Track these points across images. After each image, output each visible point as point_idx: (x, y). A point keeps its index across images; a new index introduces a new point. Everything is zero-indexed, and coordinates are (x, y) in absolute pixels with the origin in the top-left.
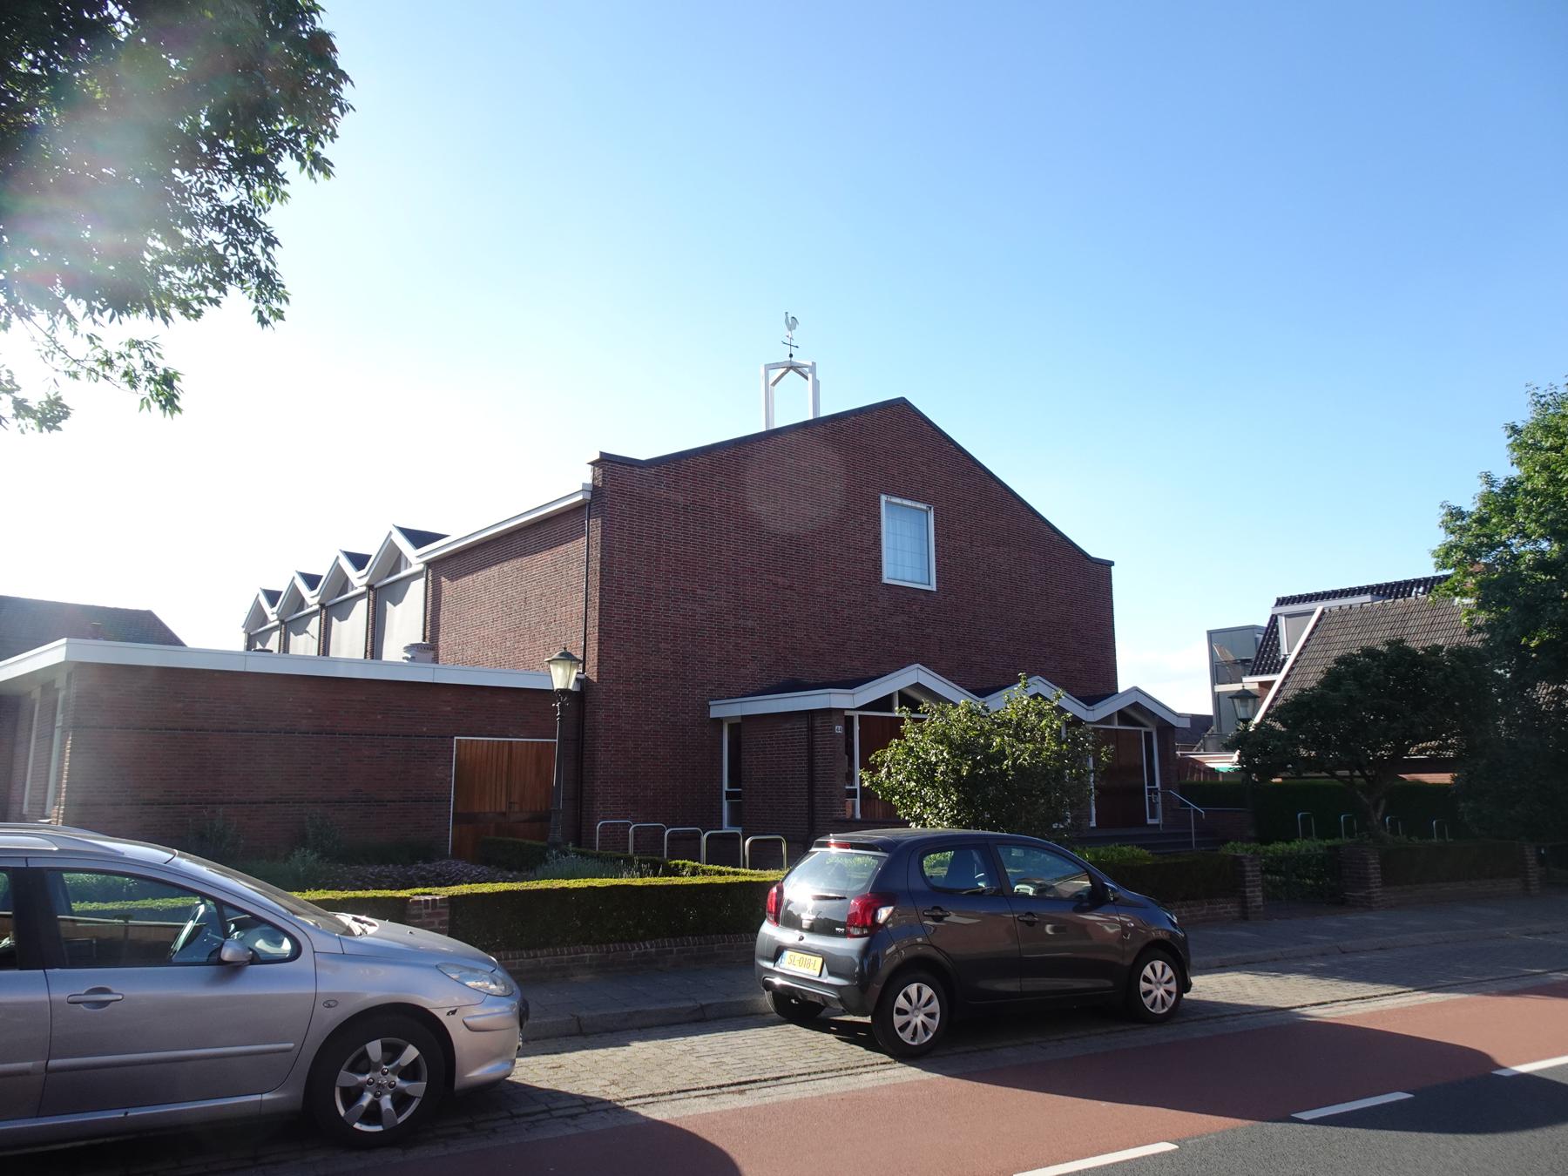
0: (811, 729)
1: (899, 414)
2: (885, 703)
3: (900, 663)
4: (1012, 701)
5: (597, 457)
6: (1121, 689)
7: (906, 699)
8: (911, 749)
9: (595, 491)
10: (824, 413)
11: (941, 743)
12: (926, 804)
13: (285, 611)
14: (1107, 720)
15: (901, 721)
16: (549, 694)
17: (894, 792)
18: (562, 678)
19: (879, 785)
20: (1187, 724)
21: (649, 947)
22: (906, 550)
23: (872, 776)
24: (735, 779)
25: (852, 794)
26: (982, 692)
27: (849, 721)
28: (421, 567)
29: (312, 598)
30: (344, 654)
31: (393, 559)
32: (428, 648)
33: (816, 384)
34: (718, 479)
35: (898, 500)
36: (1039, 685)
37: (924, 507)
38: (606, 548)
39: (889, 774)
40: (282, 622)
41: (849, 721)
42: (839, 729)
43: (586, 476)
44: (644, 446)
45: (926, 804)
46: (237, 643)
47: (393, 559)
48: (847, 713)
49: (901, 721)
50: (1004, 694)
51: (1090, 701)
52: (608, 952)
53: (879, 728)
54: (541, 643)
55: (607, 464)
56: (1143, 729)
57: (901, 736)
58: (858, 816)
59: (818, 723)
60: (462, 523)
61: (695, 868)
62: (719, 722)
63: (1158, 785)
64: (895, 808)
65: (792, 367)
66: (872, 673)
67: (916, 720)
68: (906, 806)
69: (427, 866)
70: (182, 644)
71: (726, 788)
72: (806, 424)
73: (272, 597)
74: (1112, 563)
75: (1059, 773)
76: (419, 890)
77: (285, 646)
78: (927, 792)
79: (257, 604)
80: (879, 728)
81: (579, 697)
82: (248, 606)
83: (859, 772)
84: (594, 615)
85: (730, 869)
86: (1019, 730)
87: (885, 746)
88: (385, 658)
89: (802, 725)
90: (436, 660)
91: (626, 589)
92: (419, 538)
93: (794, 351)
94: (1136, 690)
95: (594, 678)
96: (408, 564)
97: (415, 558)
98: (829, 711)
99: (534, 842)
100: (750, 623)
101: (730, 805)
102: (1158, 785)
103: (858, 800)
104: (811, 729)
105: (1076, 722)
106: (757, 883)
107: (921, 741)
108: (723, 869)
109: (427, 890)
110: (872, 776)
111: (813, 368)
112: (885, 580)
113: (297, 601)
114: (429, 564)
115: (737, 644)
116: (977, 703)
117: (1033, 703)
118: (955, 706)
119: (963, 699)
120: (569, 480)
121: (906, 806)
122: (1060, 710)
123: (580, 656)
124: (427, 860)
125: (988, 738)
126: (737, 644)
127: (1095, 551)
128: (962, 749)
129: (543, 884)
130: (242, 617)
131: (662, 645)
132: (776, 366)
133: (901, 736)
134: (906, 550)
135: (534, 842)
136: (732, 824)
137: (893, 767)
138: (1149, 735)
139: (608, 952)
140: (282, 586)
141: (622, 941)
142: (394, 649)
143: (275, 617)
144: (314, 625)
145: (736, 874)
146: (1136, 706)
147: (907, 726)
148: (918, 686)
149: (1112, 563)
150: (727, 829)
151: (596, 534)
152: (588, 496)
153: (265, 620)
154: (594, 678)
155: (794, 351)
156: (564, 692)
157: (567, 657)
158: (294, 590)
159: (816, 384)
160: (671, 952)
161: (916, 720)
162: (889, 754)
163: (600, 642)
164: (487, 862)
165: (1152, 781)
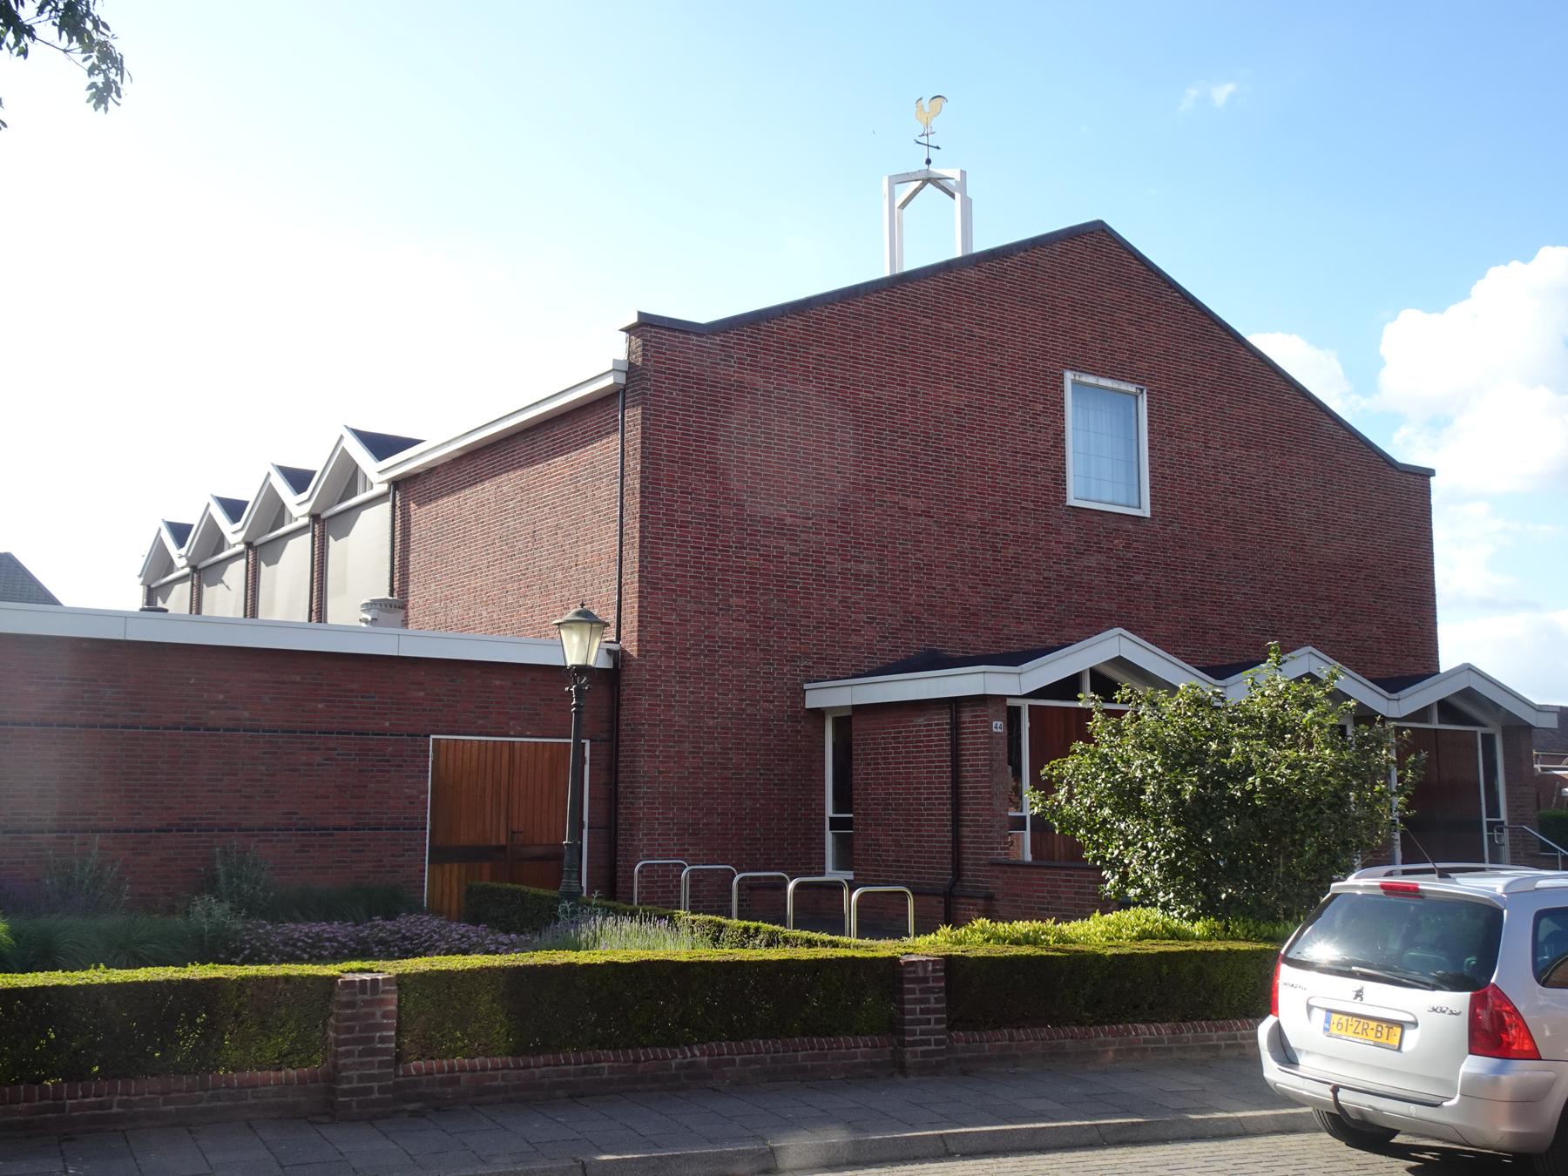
0: (956, 727)
1: (1094, 247)
2: (1068, 687)
3: (1094, 625)
4: (1261, 686)
5: (634, 319)
6: (1443, 668)
7: (1103, 684)
8: (1105, 758)
9: (631, 371)
10: (981, 244)
11: (1152, 749)
12: (1127, 844)
13: (192, 555)
14: (1422, 714)
15: (1088, 714)
16: (558, 673)
17: (1077, 823)
18: (578, 650)
19: (1055, 811)
20: (1551, 722)
21: (698, 1055)
22: (1104, 457)
23: (1045, 798)
24: (844, 798)
25: (1019, 823)
26: (1220, 672)
27: (1013, 715)
28: (384, 488)
29: (234, 534)
30: (278, 615)
31: (347, 478)
32: (394, 607)
33: (967, 205)
34: (815, 350)
35: (1091, 380)
36: (1307, 660)
37: (1132, 388)
38: (649, 456)
39: (1070, 797)
40: (194, 569)
41: (1013, 715)
42: (998, 726)
43: (617, 349)
44: (704, 305)
45: (1127, 844)
46: (132, 599)
47: (347, 478)
48: (1010, 702)
49: (1088, 714)
50: (1246, 677)
51: (1393, 684)
52: (637, 1061)
53: (1057, 725)
54: (552, 595)
55: (648, 328)
56: (1480, 730)
57: (1089, 739)
58: (1028, 857)
59: (966, 717)
60: (440, 430)
61: (773, 933)
62: (819, 713)
63: (1503, 817)
64: (1081, 848)
65: (935, 181)
66: (1050, 642)
67: (1109, 713)
68: (1097, 846)
69: (389, 925)
70: (55, 602)
71: (829, 812)
72: (948, 266)
73: (180, 532)
74: (1429, 473)
75: (1339, 801)
76: (355, 965)
77: (197, 604)
78: (1130, 825)
79: (159, 547)
80: (1057, 725)
81: (609, 681)
82: (146, 546)
83: (1029, 796)
84: (632, 555)
85: (826, 937)
86: (1276, 731)
87: (1065, 752)
88: (330, 621)
89: (944, 718)
90: (405, 623)
91: (678, 516)
92: (382, 446)
93: (933, 154)
94: (1469, 668)
95: (632, 650)
96: (368, 485)
97: (376, 473)
98: (983, 700)
99: (542, 892)
100: (865, 568)
101: (839, 839)
102: (1503, 817)
103: (1028, 833)
104: (956, 727)
105: (1365, 716)
106: (864, 960)
107: (1121, 747)
108: (815, 936)
109: (366, 965)
110: (1045, 798)
111: (963, 184)
112: (1071, 502)
113: (215, 540)
114: (396, 484)
115: (844, 599)
116: (1207, 687)
117: (1295, 688)
118: (1173, 690)
119: (1186, 678)
120: (592, 357)
121: (1097, 846)
122: (1338, 697)
123: (611, 618)
124: (390, 915)
125: (1225, 741)
126: (844, 599)
127: (1404, 449)
128: (1184, 755)
129: (540, 958)
130: (138, 562)
131: (734, 600)
132: (905, 178)
133: (1089, 739)
134: (1104, 457)
135: (542, 892)
136: (841, 865)
137: (1078, 785)
138: (1488, 740)
139: (637, 1061)
140: (191, 516)
141: (657, 1044)
142: (346, 609)
143: (183, 562)
144: (236, 573)
145: (835, 945)
146: (1468, 694)
147: (1096, 723)
148: (1120, 662)
149: (1429, 473)
150: (832, 874)
151: (634, 434)
152: (622, 379)
153: (170, 566)
154: (632, 650)
155: (933, 154)
156: (582, 670)
157: (587, 618)
158: (211, 528)
159: (967, 205)
160: (732, 1063)
161: (1109, 713)
162: (1070, 765)
163: (642, 596)
164: (475, 920)
165: (1493, 810)
